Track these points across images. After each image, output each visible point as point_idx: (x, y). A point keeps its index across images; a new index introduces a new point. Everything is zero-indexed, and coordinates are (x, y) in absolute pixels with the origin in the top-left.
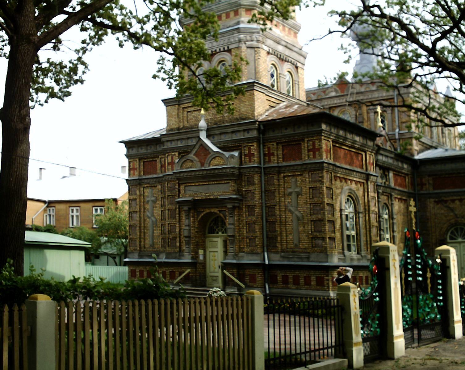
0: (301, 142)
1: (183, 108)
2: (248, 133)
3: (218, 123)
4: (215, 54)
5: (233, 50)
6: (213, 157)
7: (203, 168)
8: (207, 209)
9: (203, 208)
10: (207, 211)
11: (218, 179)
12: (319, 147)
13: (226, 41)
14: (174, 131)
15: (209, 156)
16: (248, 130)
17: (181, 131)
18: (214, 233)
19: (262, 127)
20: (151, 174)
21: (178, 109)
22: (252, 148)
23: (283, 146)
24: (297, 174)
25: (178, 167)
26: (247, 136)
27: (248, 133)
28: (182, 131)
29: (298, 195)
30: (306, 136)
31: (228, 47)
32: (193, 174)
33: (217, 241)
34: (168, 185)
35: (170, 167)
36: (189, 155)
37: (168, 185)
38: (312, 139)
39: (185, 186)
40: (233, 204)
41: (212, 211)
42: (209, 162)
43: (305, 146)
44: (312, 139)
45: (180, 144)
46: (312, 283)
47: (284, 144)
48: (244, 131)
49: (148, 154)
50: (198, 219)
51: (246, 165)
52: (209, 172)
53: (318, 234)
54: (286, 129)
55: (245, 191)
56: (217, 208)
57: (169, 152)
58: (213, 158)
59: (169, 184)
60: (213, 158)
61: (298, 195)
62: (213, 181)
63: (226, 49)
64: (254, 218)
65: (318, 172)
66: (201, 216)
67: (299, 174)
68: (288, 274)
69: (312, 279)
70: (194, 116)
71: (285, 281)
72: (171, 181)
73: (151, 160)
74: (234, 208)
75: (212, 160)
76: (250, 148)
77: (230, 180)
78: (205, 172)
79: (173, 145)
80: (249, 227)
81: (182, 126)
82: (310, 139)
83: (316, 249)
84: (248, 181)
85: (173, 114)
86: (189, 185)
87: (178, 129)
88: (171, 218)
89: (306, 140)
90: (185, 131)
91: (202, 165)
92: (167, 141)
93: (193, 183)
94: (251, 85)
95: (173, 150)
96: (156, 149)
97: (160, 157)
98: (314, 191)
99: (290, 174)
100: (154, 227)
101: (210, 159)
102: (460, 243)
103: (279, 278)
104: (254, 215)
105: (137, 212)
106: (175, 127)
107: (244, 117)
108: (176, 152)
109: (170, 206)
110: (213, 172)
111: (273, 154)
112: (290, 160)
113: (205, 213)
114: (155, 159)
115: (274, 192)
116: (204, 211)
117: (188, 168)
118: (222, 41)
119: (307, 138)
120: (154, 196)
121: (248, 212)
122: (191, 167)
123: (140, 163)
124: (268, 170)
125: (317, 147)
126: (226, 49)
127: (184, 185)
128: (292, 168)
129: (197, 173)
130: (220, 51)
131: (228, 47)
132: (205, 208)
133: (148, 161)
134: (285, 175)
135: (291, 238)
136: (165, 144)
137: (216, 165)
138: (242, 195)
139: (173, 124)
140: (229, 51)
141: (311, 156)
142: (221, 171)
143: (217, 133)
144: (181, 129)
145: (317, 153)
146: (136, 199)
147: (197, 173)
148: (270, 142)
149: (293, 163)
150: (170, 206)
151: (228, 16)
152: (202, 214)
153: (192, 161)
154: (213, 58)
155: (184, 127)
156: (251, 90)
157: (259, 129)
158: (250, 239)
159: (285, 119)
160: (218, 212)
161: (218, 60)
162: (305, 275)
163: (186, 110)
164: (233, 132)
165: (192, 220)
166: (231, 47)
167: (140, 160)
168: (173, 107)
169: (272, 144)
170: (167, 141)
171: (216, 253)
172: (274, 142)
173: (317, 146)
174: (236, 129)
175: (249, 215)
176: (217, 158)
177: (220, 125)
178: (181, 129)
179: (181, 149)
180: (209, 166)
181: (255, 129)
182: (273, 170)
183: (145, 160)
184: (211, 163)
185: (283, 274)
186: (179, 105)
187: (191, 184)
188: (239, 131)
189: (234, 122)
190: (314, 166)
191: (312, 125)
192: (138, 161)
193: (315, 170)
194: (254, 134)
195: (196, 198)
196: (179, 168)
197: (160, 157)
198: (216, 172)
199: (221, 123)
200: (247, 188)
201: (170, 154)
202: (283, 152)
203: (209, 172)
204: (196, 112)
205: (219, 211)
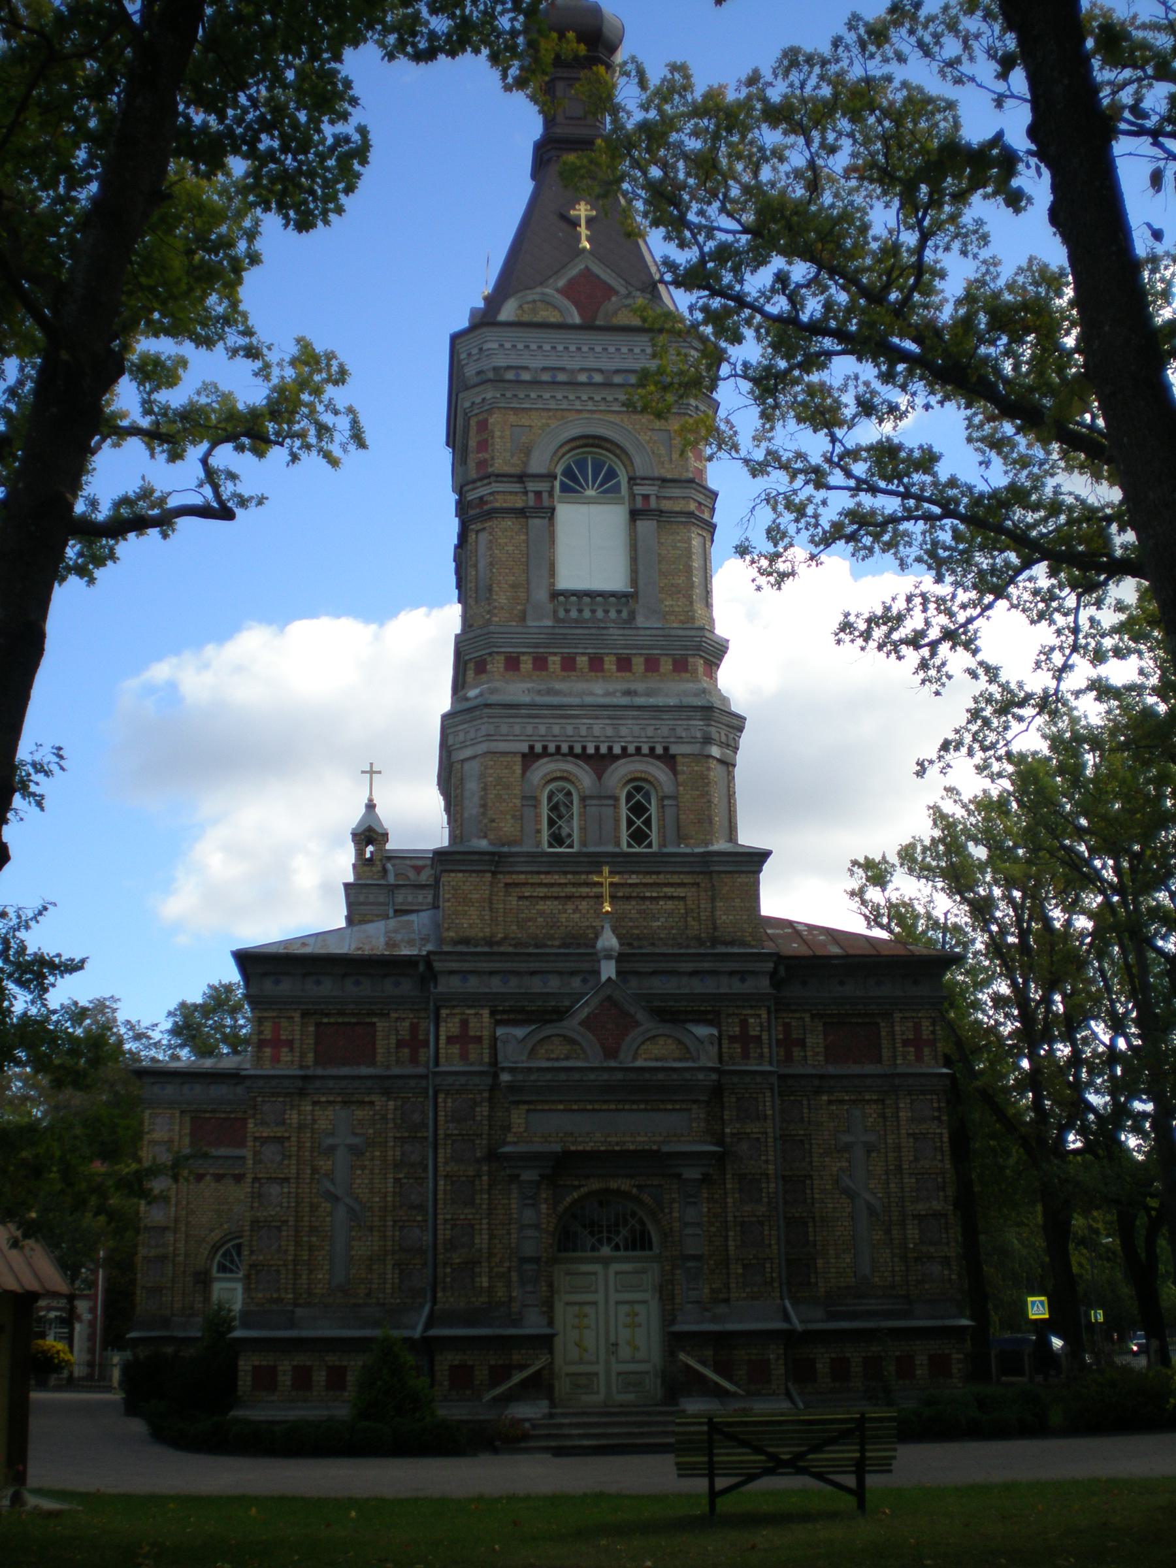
2: (743, 980)
3: (635, 943)
4: (539, 756)
6: (651, 1034)
7: (613, 1064)
10: (596, 1185)
11: (534, 1098)
12: (931, 1037)
13: (665, 731)
14: (476, 946)
16: (743, 975)
17: (495, 949)
18: (574, 1251)
21: (492, 884)
22: (751, 1020)
23: (825, 1024)
26: (737, 987)
27: (743, 980)
28: (502, 949)
29: (869, 1152)
32: (577, 1076)
33: (595, 1274)
34: (445, 1102)
35: (455, 1050)
36: (565, 1023)
37: (445, 1102)
38: (914, 1015)
39: (528, 1111)
41: (613, 1185)
44: (914, 1015)
45: (495, 985)
46: (919, 1372)
51: (733, 1064)
53: (932, 1249)
55: (733, 1134)
57: (454, 1007)
58: (648, 1039)
60: (648, 1039)
61: (869, 1152)
63: (659, 750)
65: (929, 1097)
66: (569, 1200)
67: (875, 1097)
68: (848, 1355)
69: (918, 1362)
70: (541, 913)
71: (302, 1379)
73: (354, 1020)
74: (706, 1179)
75: (643, 1043)
77: (695, 1102)
79: (473, 985)
82: (907, 1015)
83: (927, 1286)
86: (546, 1107)
87: (490, 942)
89: (897, 1016)
90: (510, 949)
92: (452, 973)
93: (561, 1102)
95: (473, 1000)
97: (394, 1015)
99: (846, 1098)
102: (606, 1262)
103: (822, 1367)
106: (481, 935)
108: (482, 1007)
111: (906, 1043)
113: (583, 1190)
114: (368, 1020)
115: (802, 1141)
116: (579, 1187)
117: (557, 1059)
118: (652, 728)
119: (901, 1010)
120: (355, 1134)
122: (567, 1058)
125: (925, 1037)
127: (526, 1107)
129: (592, 1076)
130: (545, 753)
131: (666, 749)
133: (336, 1024)
135: (848, 1260)
136: (442, 980)
137: (657, 1060)
138: (720, 1142)
139: (471, 926)
140: (669, 759)
141: (912, 1058)
144: (499, 943)
145: (926, 1051)
147: (592, 1076)
149: (856, 1069)
151: (652, 665)
152: (575, 1195)
153: (572, 1041)
155: (505, 938)
156: (750, 872)
157: (773, 975)
158: (745, 1267)
160: (634, 1190)
162: (898, 1353)
164: (694, 973)
165: (544, 1211)
166: (674, 750)
167: (305, 1014)
168: (474, 878)
169: (797, 1015)
170: (452, 973)
171: (587, 1309)
174: (706, 965)
176: (661, 1041)
177: (640, 947)
178: (499, 943)
180: (635, 1059)
184: (640, 1051)
185: (833, 1355)
186: (494, 873)
187: (553, 1107)
189: (688, 947)
192: (297, 1019)
194: (764, 985)
195: (573, 1148)
196: (524, 1058)
197: (394, 1015)
198: (661, 1076)
200: (738, 1126)
205: (639, 1187)
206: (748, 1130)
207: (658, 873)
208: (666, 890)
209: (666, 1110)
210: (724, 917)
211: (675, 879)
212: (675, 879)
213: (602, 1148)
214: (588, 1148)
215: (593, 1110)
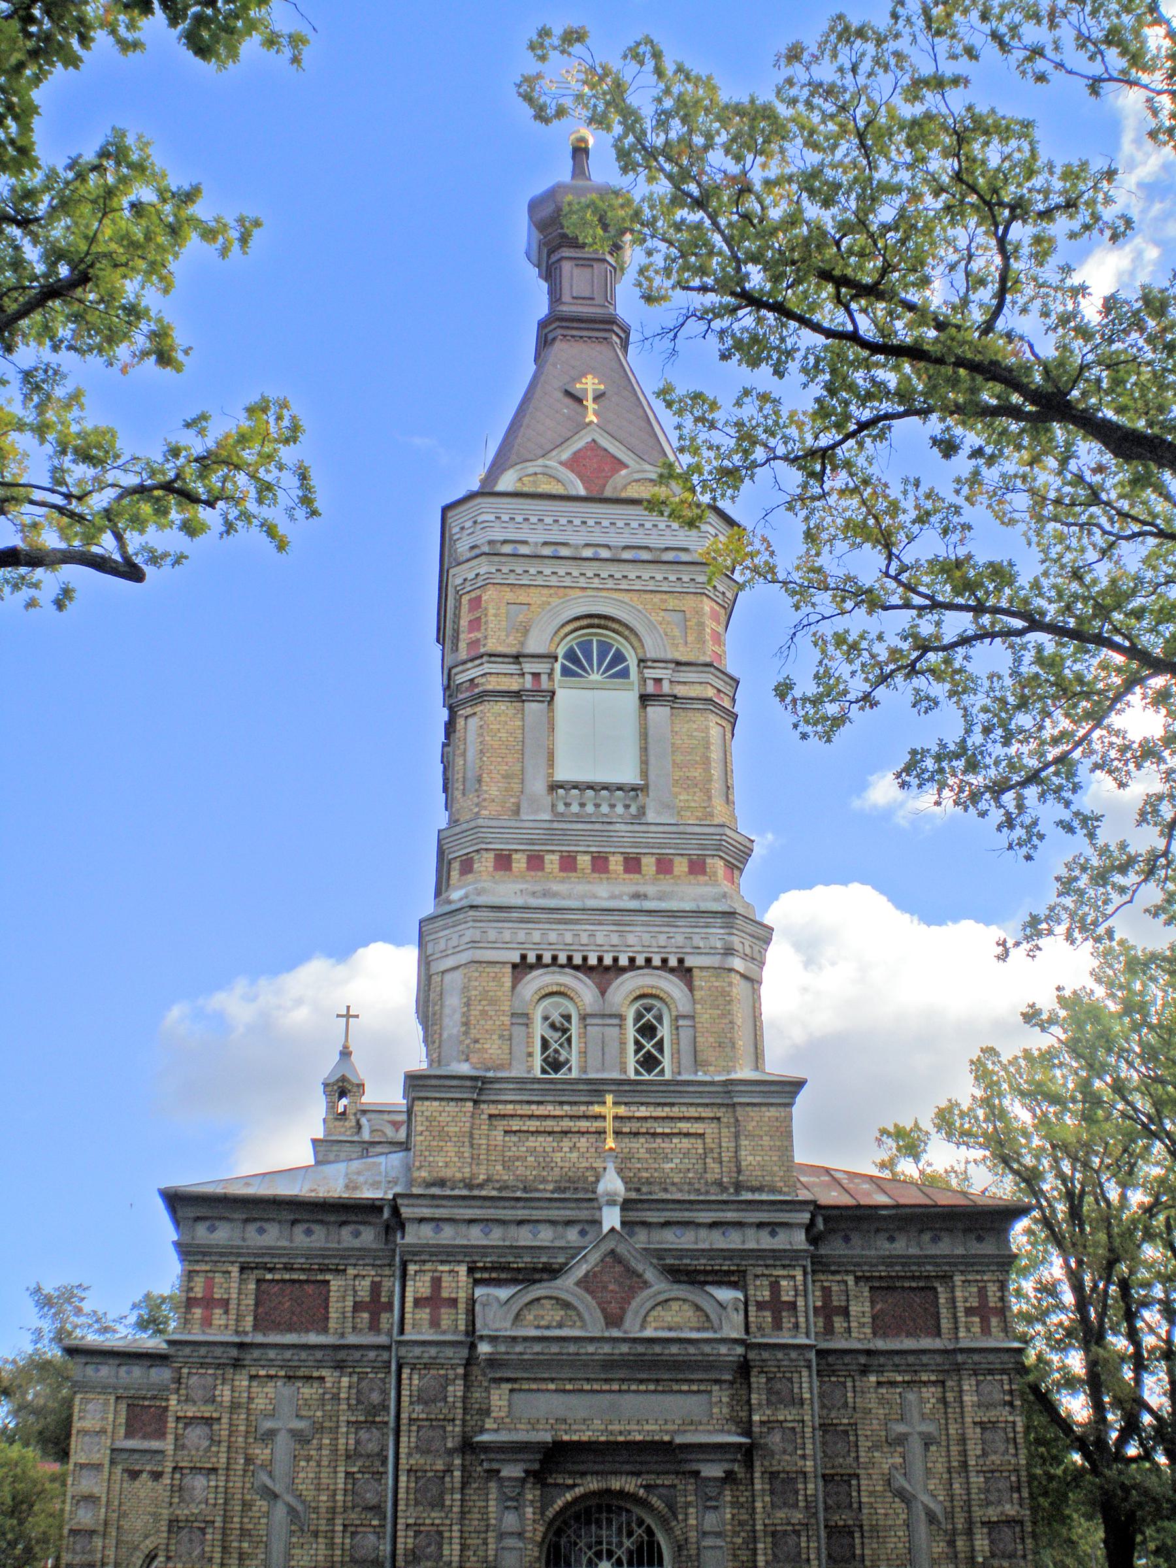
0: (937, 1285)
1: (491, 1116)
2: (773, 1234)
5: (696, 972)
6: (661, 1298)
8: (589, 1478)
9: (572, 1474)
10: (593, 1484)
15: (646, 1293)
17: (476, 1193)
19: (820, 1222)
20: (290, 1329)
24: (924, 1378)
25: (505, 1319)
26: (766, 1241)
28: (484, 1193)
30: (962, 1268)
31: (681, 961)
39: (511, 1391)
40: (727, 1466)
41: (616, 1484)
42: (643, 1312)
43: (965, 1295)
45: (475, 1236)
47: (876, 1284)
48: (760, 1225)
49: (296, 1256)
50: (550, 1513)
52: (640, 1349)
54: (891, 1239)
55: (762, 1423)
56: (638, 1474)
59: (416, 1377)
62: (641, 1381)
64: (798, 1516)
66: (560, 1503)
70: (532, 1151)
72: (427, 1366)
73: (303, 1277)
75: (653, 1308)
76: (777, 1282)
78: (625, 1348)
79: (448, 1235)
80: (774, 1544)
81: (482, 1177)
84: (770, 1391)
85: (453, 1129)
88: (417, 1503)
91: (613, 1320)
92: (421, 1220)
94: (787, 1089)
95: (447, 1254)
96: (291, 1241)
98: (988, 1435)
99: (899, 1379)
100: (292, 1533)
101: (649, 1305)
104: (795, 1505)
105: (214, 1470)
106: (459, 1175)
107: (757, 1184)
109: (417, 1460)
110: (572, 1349)
111: (969, 1311)
112: (897, 1335)
113: (578, 1491)
116: (574, 1486)
117: (548, 1327)
121: (772, 1492)
122: (560, 1326)
123: (242, 1282)
124: (831, 1359)
126: (673, 962)
128: (911, 1359)
129: (591, 1349)
131: (681, 961)
132: (583, 1474)
134: (882, 1379)
137: (670, 1329)
140: (684, 972)
141: (976, 1329)
142: (692, 1350)
143: (655, 1220)
144: (481, 1186)
145: (994, 1321)
146: (209, 1421)
148: (834, 1273)
149: (909, 1344)
150: (417, 1460)
152: (569, 1497)
154: (529, 977)
155: (488, 1180)
159: (900, 1211)
160: (642, 1491)
161: (565, 986)
163: (502, 1125)
168: (452, 1107)
169: (838, 1278)
170: (421, 1220)
172: (847, 1272)
173: (993, 1302)
174: (730, 1216)
175: (773, 1506)
176: (675, 1306)
178: (481, 1186)
179: (485, 1255)
181: (799, 1225)
182: (847, 1359)
183: (269, 1276)
187: (543, 1387)
188: (739, 1225)
190: (991, 1358)
191: (980, 1239)
193: (991, 1372)
194: (799, 1239)
195: (566, 1438)
196: (508, 1324)
197: (351, 1271)
198: (674, 1349)
199: (656, 1188)
200: (768, 1412)
201: (428, 1267)
202: (872, 1308)
203: (640, 1349)
204: (540, 1139)
205: (647, 1487)
206: (781, 1418)
207: (672, 1105)
208: (680, 1125)
209: (680, 1392)
210: (750, 1158)
211: (692, 1112)
212: (692, 1112)
213: (603, 1439)
214: (585, 1438)
215: (592, 1391)
